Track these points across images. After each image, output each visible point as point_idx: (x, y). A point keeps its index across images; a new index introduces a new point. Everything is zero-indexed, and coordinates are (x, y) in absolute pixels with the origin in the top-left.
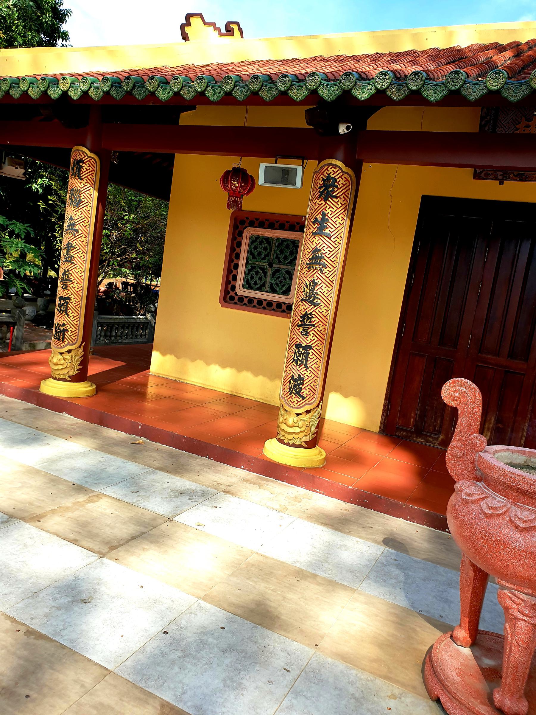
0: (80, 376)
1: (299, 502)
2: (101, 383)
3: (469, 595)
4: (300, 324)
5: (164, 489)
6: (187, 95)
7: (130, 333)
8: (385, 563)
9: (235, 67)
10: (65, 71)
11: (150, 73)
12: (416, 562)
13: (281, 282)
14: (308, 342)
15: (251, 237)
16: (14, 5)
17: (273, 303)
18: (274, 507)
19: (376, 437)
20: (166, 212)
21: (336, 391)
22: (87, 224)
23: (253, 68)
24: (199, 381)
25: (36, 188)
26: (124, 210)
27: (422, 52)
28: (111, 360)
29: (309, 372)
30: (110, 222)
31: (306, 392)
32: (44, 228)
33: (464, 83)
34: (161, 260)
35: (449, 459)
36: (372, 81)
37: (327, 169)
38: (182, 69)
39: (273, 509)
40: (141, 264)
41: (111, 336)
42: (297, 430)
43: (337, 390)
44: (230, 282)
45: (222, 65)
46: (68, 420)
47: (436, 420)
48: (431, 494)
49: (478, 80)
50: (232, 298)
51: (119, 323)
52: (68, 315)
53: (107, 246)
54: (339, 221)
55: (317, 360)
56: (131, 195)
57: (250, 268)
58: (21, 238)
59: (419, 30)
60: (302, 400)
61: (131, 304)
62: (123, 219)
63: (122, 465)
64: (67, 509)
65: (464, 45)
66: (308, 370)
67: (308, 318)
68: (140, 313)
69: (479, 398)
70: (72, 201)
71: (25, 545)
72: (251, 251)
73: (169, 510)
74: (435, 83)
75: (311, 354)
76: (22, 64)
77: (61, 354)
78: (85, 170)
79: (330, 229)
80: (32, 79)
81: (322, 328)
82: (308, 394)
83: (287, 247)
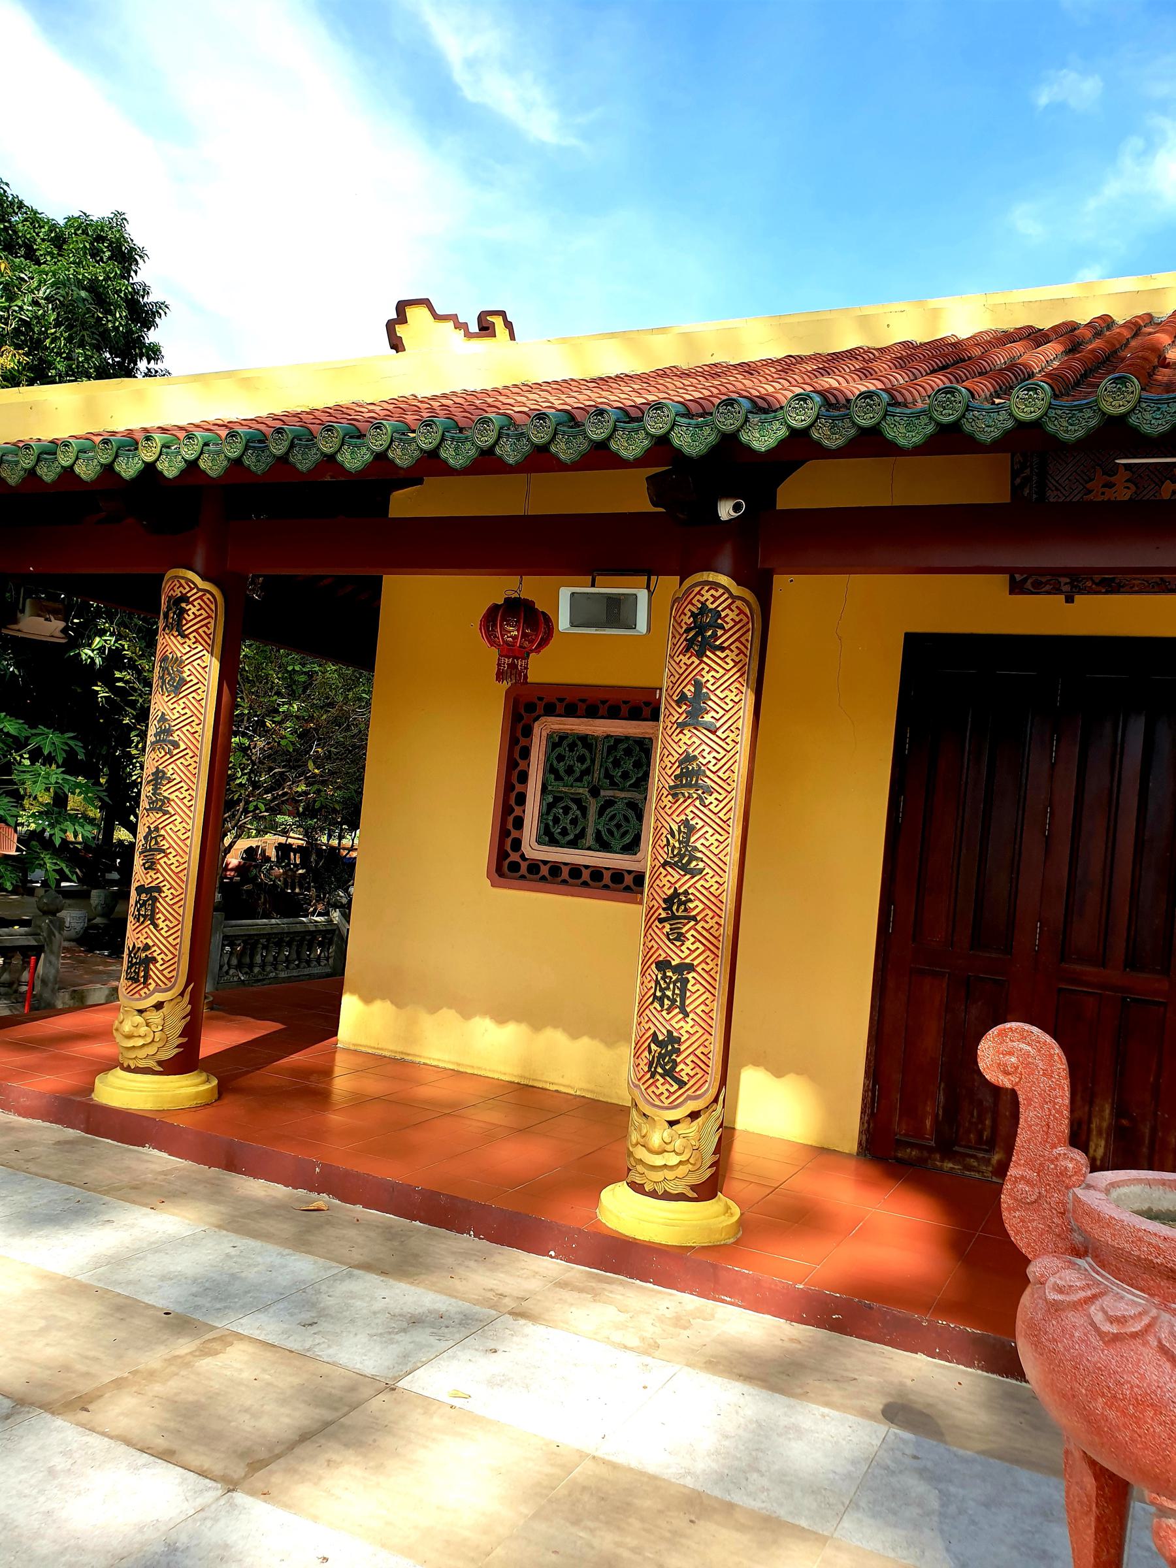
0: (183, 1061)
1: (685, 1328)
2: (230, 1074)
3: (1089, 1536)
4: (664, 915)
5: (375, 1313)
6: (402, 457)
7: (294, 956)
8: (892, 1465)
9: (501, 398)
10: (152, 421)
11: (325, 418)
12: (964, 1460)
13: (618, 826)
14: (683, 956)
15: (549, 737)
16: (48, 299)
17: (604, 871)
18: (629, 1345)
19: (852, 1164)
20: (370, 692)
21: (756, 1064)
22: (197, 728)
23: (536, 397)
24: (446, 1058)
25: (90, 657)
26: (278, 694)
27: (881, 350)
28: (252, 1020)
29: (691, 1023)
30: (249, 719)
31: (687, 1070)
32: (105, 740)
33: (967, 410)
34: (360, 793)
35: (1009, 1209)
36: (780, 414)
37: (699, 593)
38: (390, 407)
39: (625, 1347)
40: (317, 805)
41: (251, 966)
42: (673, 1160)
43: (758, 1061)
44: (508, 833)
45: (473, 394)
46: (156, 1161)
47: (981, 1120)
48: (979, 1292)
49: (993, 403)
50: (514, 867)
51: (269, 936)
52: (156, 926)
53: (242, 770)
54: (732, 696)
55: (707, 995)
56: (294, 662)
57: (551, 800)
58: (56, 763)
59: (869, 310)
60: (680, 1088)
61: (297, 890)
62: (276, 711)
63: (278, 1261)
64: (151, 1375)
65: (964, 333)
66: (688, 1020)
67: (681, 903)
68: (315, 910)
69: (1061, 1065)
70: (164, 682)
71: (52, 1472)
72: (551, 765)
73: (386, 1364)
74: (909, 411)
75: (692, 981)
76: (64, 414)
77: (140, 1012)
78: (192, 616)
79: (713, 713)
80: (83, 444)
81: (712, 923)
82: (692, 1073)
83: (628, 752)
